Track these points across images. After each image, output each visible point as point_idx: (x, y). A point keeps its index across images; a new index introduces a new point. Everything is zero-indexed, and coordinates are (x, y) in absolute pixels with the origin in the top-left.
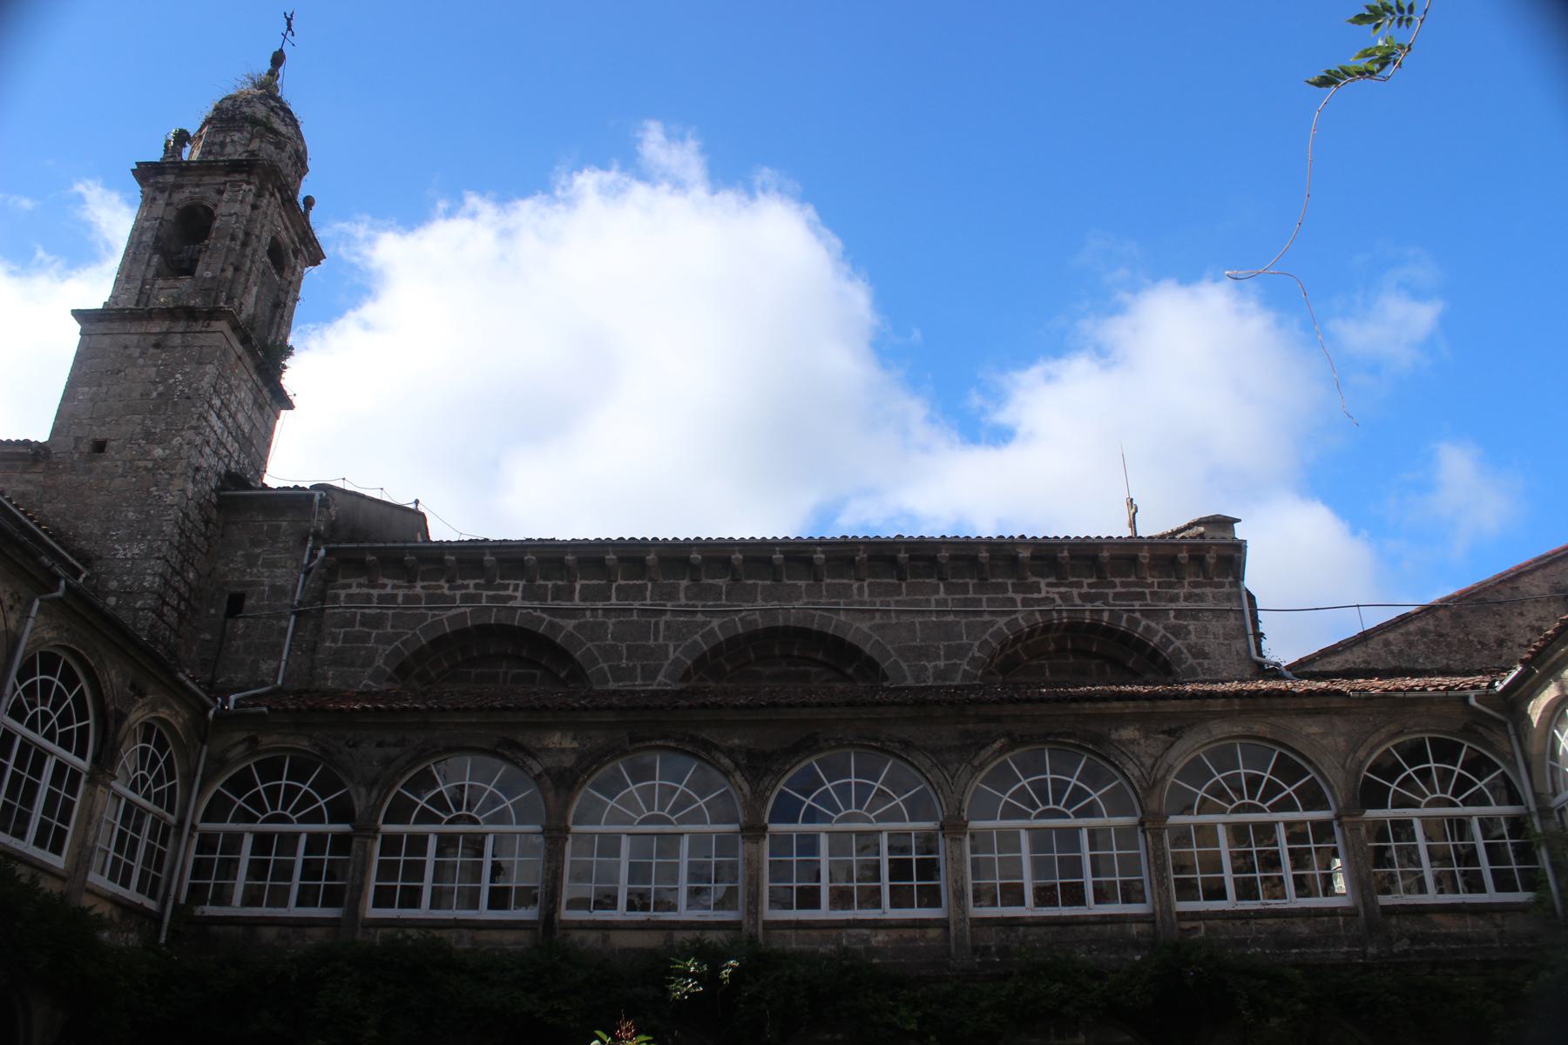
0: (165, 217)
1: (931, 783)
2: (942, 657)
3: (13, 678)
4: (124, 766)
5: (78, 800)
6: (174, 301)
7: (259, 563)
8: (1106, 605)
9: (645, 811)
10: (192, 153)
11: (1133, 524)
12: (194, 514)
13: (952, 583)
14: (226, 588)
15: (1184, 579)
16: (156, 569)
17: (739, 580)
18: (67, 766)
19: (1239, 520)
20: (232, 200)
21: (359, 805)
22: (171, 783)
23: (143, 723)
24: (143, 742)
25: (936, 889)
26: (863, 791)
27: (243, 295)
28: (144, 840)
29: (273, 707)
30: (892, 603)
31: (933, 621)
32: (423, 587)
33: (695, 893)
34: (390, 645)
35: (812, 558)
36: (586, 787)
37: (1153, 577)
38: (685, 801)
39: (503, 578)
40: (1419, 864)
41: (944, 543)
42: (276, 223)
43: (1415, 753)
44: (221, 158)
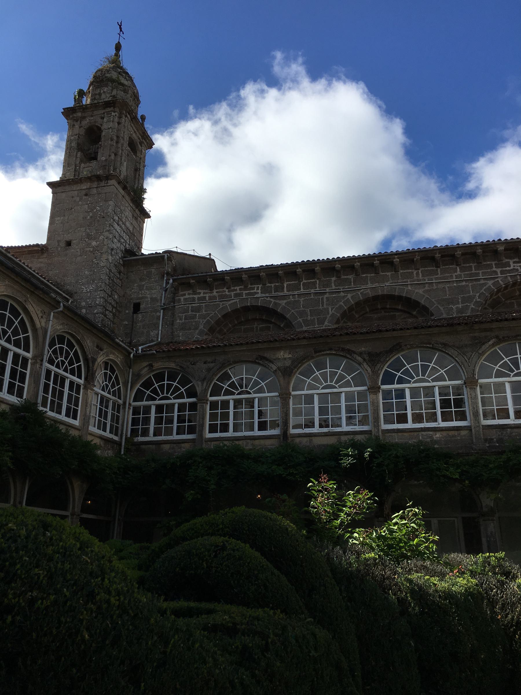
0: (81, 134)
2: (460, 303)
6: (90, 173)
10: (87, 100)
12: (114, 270)
17: (359, 275)
18: (74, 383)
20: (108, 121)
21: (199, 390)
23: (103, 362)
25: (464, 412)
26: (425, 368)
27: (120, 167)
29: (158, 350)
30: (434, 279)
31: (454, 286)
32: (216, 292)
33: (349, 418)
34: (205, 319)
35: (393, 261)
36: (297, 375)
38: (342, 377)
39: (251, 285)
41: (458, 247)
44: (100, 101)
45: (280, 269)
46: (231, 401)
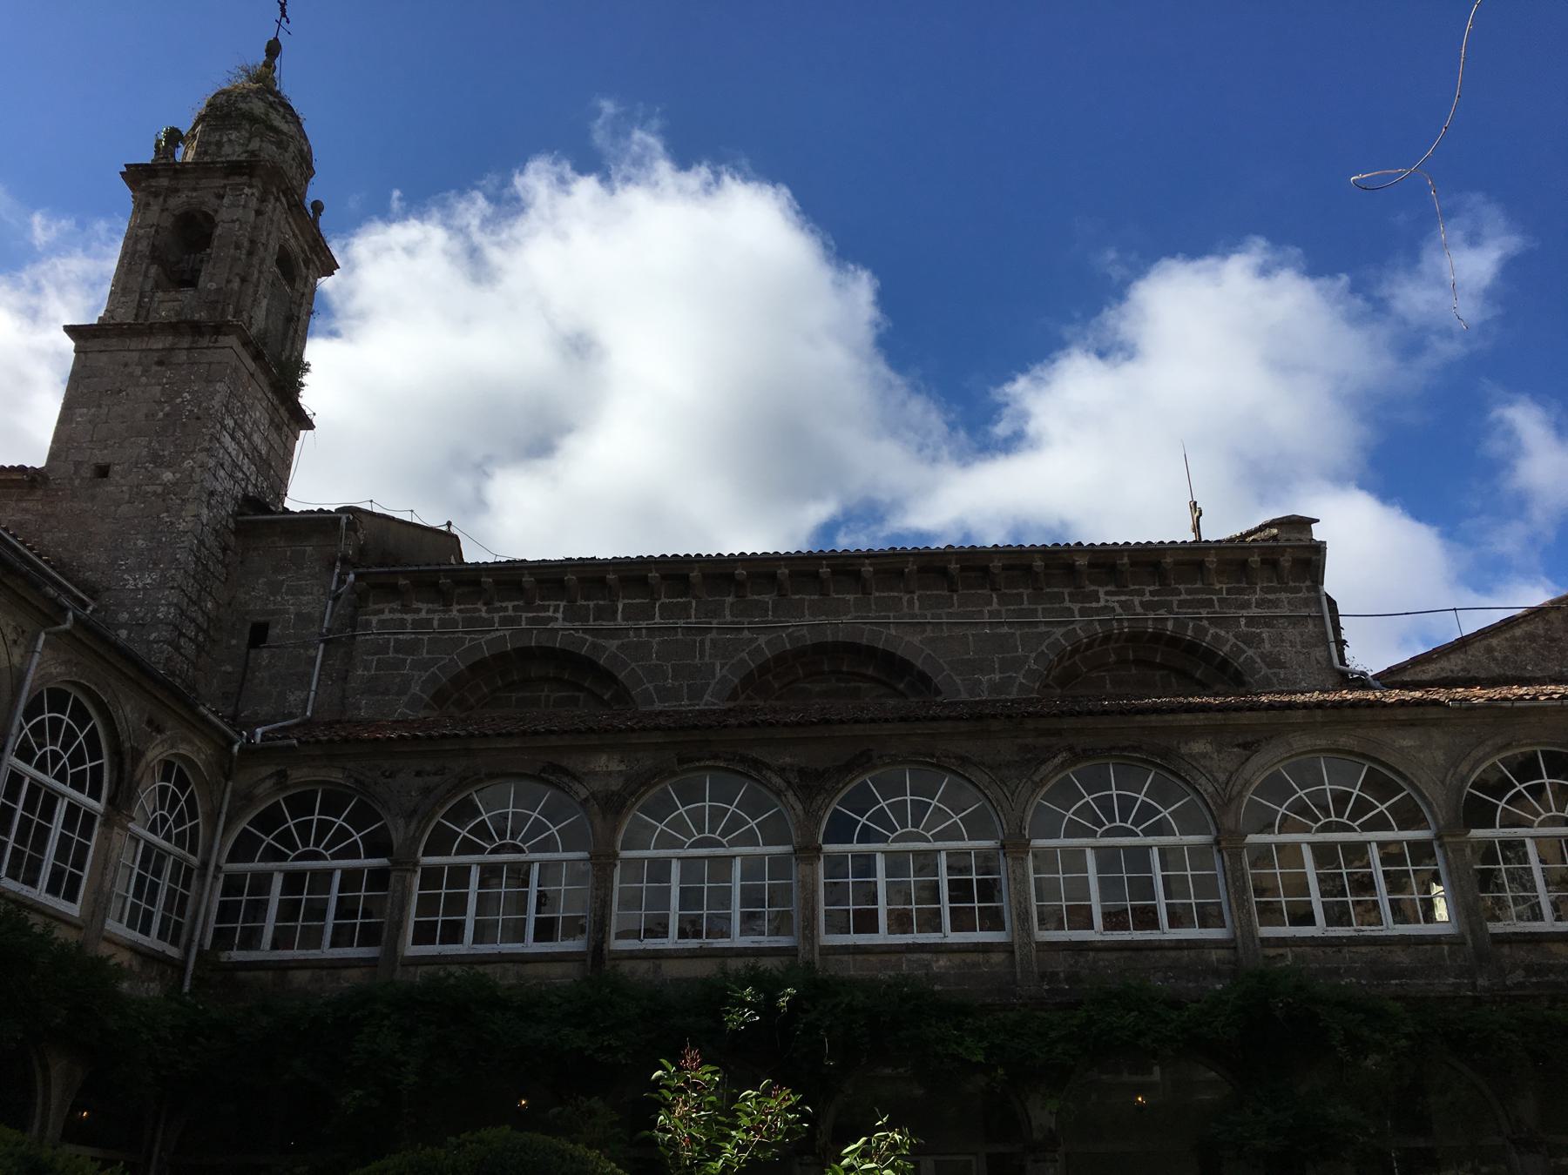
1: (991, 801)
3: (19, 717)
4: (142, 807)
5: (93, 844)
7: (284, 590)
8: (1170, 614)
9: (696, 834)
10: (186, 153)
11: (1196, 528)
12: (210, 541)
13: (1006, 593)
14: (247, 617)
15: (1257, 584)
16: (171, 599)
19: (1318, 521)
20: (233, 205)
21: (397, 838)
22: (193, 823)
23: (160, 760)
24: (161, 781)
26: (920, 808)
28: (164, 883)
33: (748, 918)
37: (1220, 582)
40: (1534, 889)
42: (283, 231)
43: (1526, 768)
44: (219, 159)
45: (611, 568)
46: (474, 868)
